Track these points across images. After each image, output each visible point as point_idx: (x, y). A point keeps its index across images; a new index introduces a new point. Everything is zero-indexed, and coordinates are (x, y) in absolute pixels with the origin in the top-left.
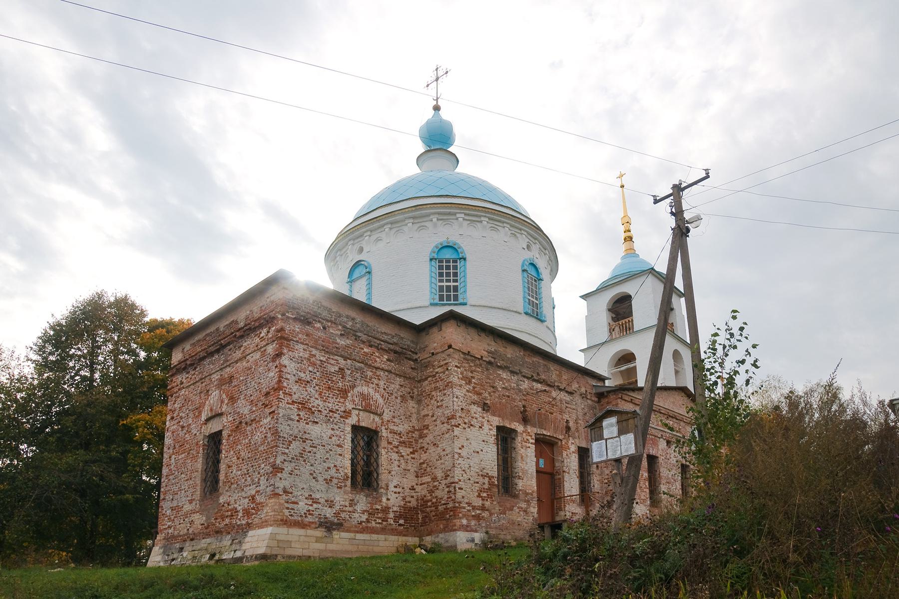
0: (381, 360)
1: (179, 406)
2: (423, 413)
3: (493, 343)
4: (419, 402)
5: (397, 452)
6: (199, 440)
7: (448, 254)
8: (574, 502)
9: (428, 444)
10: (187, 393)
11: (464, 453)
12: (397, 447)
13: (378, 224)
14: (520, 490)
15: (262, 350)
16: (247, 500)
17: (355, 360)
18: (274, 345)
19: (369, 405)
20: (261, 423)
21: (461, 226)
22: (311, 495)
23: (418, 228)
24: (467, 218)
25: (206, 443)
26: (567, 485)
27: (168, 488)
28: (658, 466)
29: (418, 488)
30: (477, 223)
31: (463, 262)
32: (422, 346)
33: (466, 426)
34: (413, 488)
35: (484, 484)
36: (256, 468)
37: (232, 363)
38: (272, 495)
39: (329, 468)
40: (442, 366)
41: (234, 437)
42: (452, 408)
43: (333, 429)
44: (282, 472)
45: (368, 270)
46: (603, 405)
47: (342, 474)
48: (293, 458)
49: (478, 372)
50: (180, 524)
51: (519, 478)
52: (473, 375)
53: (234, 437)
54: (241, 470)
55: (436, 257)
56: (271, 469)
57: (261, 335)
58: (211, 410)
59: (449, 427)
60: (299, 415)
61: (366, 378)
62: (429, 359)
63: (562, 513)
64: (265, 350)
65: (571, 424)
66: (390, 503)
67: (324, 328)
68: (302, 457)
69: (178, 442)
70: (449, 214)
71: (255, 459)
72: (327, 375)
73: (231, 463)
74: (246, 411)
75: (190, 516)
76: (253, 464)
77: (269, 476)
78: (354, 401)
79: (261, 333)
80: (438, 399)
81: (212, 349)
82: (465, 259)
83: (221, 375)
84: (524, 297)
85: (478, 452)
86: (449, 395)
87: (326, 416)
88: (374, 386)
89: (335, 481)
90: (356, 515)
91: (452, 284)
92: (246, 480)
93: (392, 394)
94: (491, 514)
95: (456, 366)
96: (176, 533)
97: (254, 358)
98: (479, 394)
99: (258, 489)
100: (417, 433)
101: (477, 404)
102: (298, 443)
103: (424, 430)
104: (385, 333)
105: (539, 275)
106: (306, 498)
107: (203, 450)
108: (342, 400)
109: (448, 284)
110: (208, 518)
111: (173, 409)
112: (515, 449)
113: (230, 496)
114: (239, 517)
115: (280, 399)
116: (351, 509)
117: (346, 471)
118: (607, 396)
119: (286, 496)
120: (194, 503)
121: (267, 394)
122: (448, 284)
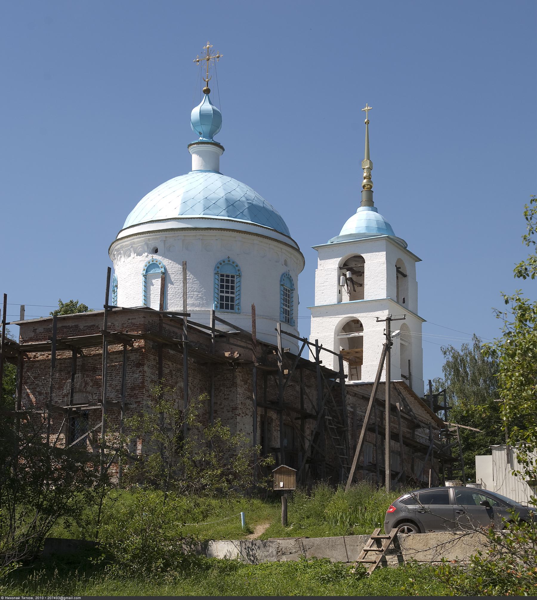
7: (228, 271)
33: (243, 415)
59: (233, 415)
80: (225, 393)
84: (281, 307)
85: (249, 434)
86: (234, 392)
91: (230, 295)
93: (195, 387)
101: (250, 398)
109: (227, 295)
115: (144, 394)
122: (227, 295)
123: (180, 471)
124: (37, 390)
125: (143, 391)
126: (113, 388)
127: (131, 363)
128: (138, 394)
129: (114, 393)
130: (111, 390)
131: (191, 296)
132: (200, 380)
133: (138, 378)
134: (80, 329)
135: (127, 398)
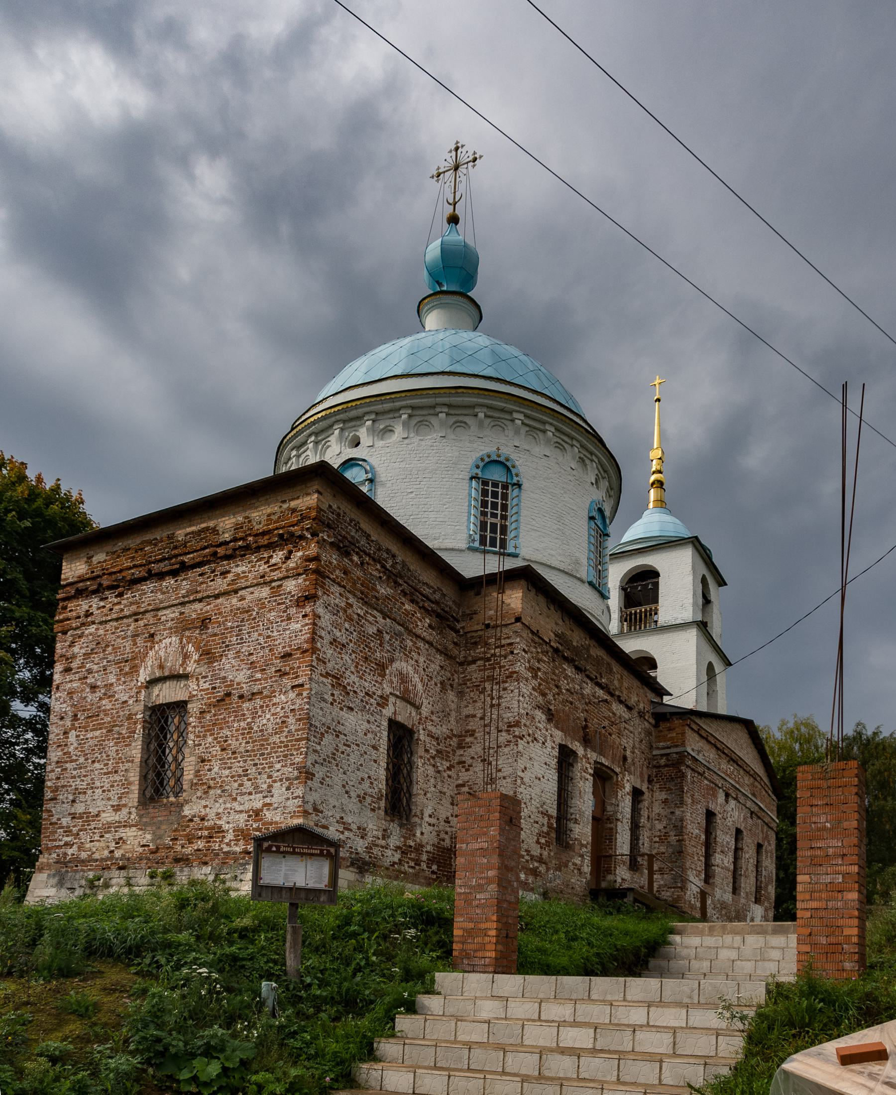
0: (423, 625)
1: (83, 651)
2: (465, 712)
3: (560, 622)
4: (461, 694)
5: (434, 766)
6: (133, 712)
7: (497, 475)
8: (624, 863)
9: (473, 758)
10: (101, 632)
11: (527, 776)
12: (433, 758)
13: (392, 404)
14: (576, 839)
15: (273, 584)
16: (244, 816)
17: (395, 620)
18: (300, 581)
19: (407, 690)
20: (275, 700)
21: (517, 432)
22: (342, 818)
23: (455, 422)
24: (527, 421)
25: (147, 717)
26: (619, 839)
27: (62, 782)
28: (714, 827)
29: (454, 820)
30: (538, 432)
31: (516, 492)
32: (468, 612)
33: (530, 739)
34: (447, 821)
35: (543, 825)
36: (264, 768)
37: (208, 597)
38: (298, 812)
39: (363, 779)
40: (503, 646)
41: (215, 715)
42: (516, 710)
43: (369, 722)
44: (312, 779)
45: (370, 476)
46: (661, 731)
47: (376, 790)
48: (324, 760)
49: (544, 662)
50: (91, 841)
51: (576, 822)
52: (539, 666)
53: (215, 715)
54: (230, 768)
55: (480, 476)
56: (296, 773)
57: (273, 561)
58: (161, 667)
60: (333, 695)
61: (406, 650)
62: (480, 633)
63: (610, 877)
64: (280, 586)
65: (628, 753)
66: (425, 839)
67: (362, 563)
68: (334, 759)
69: (84, 710)
70: (503, 410)
71: (263, 754)
72: (363, 639)
73: (206, 756)
74: (241, 676)
75: (116, 831)
76: (257, 761)
77: (291, 784)
78: (392, 682)
79: (271, 557)
81: (163, 567)
82: (519, 485)
83: (182, 613)
86: (512, 691)
87: (362, 701)
88: (413, 662)
89: (369, 800)
90: (389, 853)
92: (241, 785)
94: (548, 869)
95: (524, 650)
96: (84, 855)
97: (256, 595)
98: (544, 695)
99: (268, 800)
100: (454, 742)
102: (330, 737)
103: (466, 736)
104: (426, 583)
105: (605, 529)
106: (337, 822)
107: (144, 728)
108: (379, 680)
110: (157, 837)
111: (69, 654)
112: (572, 779)
113: (206, 807)
114: (227, 841)
116: (383, 843)
117: (380, 786)
118: (668, 720)
119: (317, 815)
120: (125, 811)
121: (287, 656)
123: (396, 851)
124: (88, 681)
125: (312, 661)
126: (243, 660)
127: (286, 598)
128: (299, 667)
129: (245, 670)
130: (239, 666)
131: (424, 520)
132: (441, 667)
133: (301, 631)
134: (179, 541)
135: (274, 679)
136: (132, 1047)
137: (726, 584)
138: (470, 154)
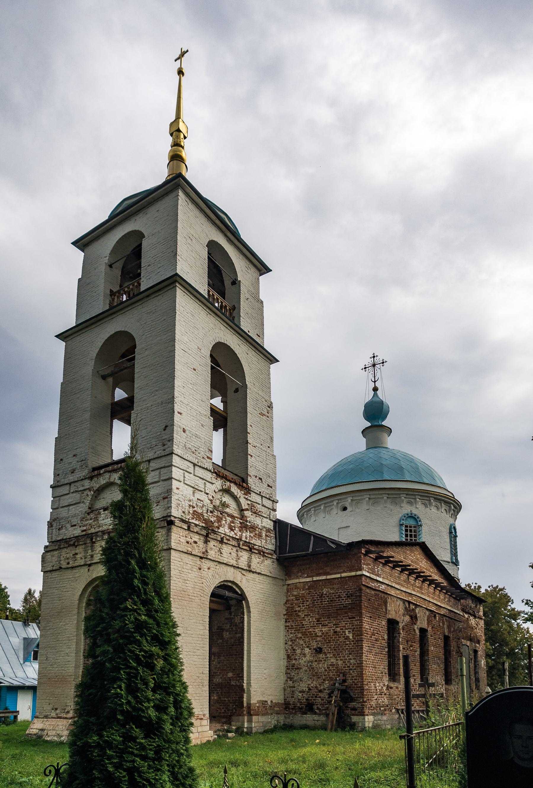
7: (411, 522)
136: (425, 716)
137: (268, 270)
138: (381, 360)
